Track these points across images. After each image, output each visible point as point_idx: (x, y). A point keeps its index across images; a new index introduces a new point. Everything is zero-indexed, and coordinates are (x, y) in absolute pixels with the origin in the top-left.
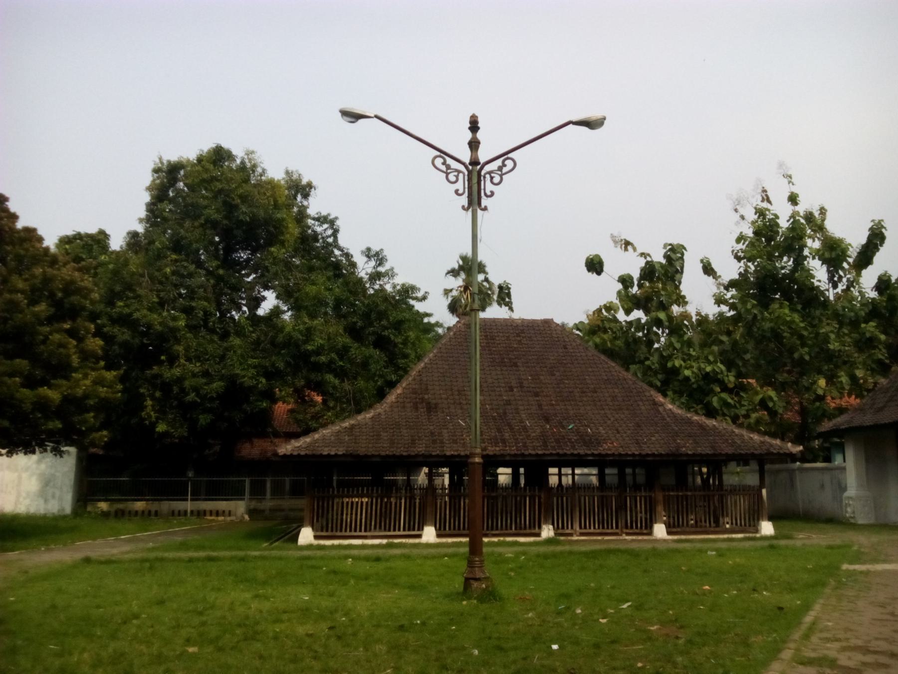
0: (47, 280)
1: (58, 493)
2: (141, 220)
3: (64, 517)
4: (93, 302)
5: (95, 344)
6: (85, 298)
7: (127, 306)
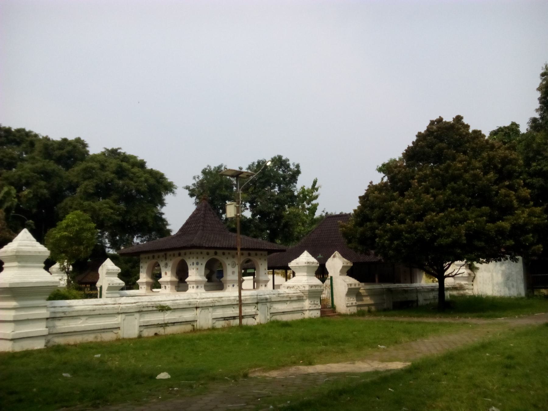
0: (491, 159)
1: (515, 284)
2: (537, 110)
3: (522, 298)
4: (520, 167)
5: (526, 192)
6: (515, 165)
7: (539, 165)
